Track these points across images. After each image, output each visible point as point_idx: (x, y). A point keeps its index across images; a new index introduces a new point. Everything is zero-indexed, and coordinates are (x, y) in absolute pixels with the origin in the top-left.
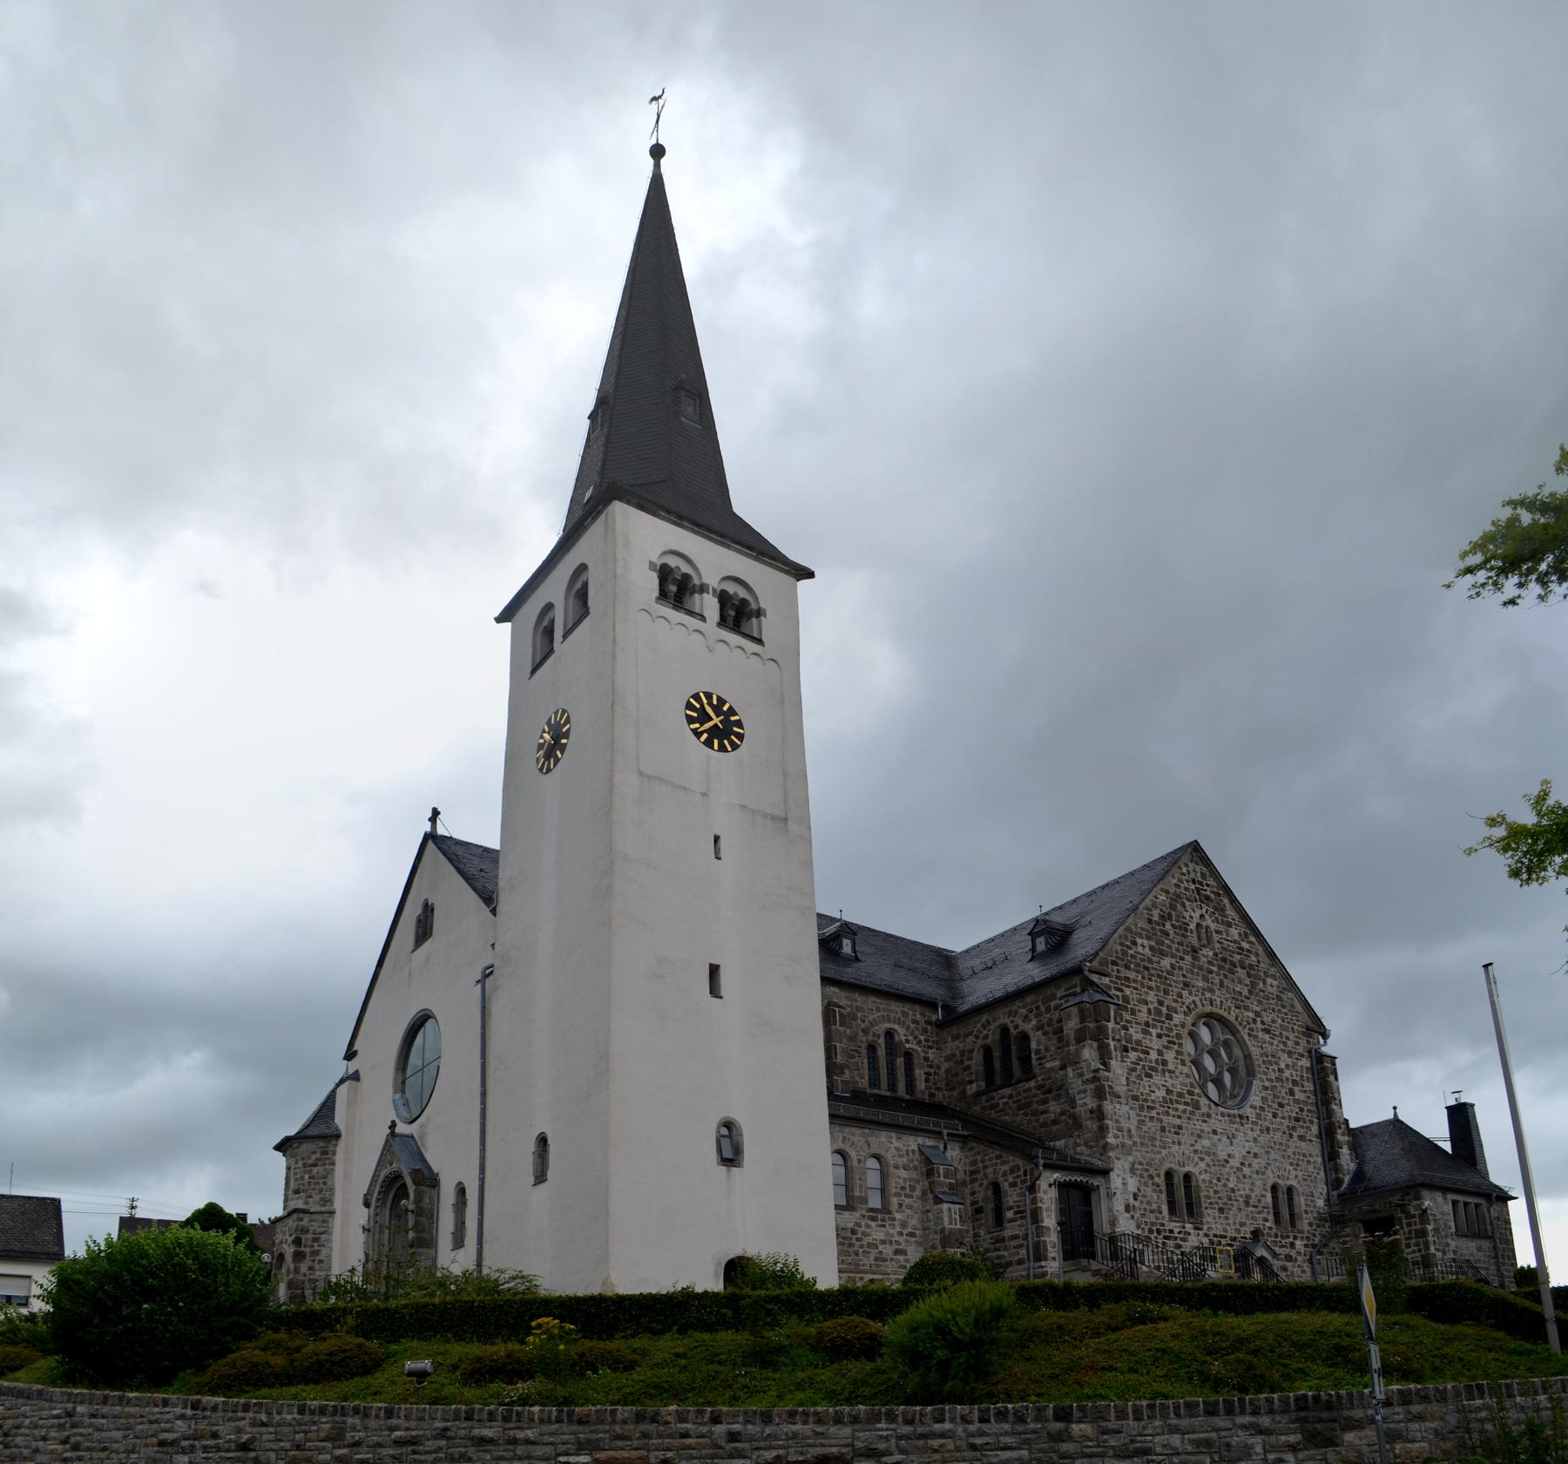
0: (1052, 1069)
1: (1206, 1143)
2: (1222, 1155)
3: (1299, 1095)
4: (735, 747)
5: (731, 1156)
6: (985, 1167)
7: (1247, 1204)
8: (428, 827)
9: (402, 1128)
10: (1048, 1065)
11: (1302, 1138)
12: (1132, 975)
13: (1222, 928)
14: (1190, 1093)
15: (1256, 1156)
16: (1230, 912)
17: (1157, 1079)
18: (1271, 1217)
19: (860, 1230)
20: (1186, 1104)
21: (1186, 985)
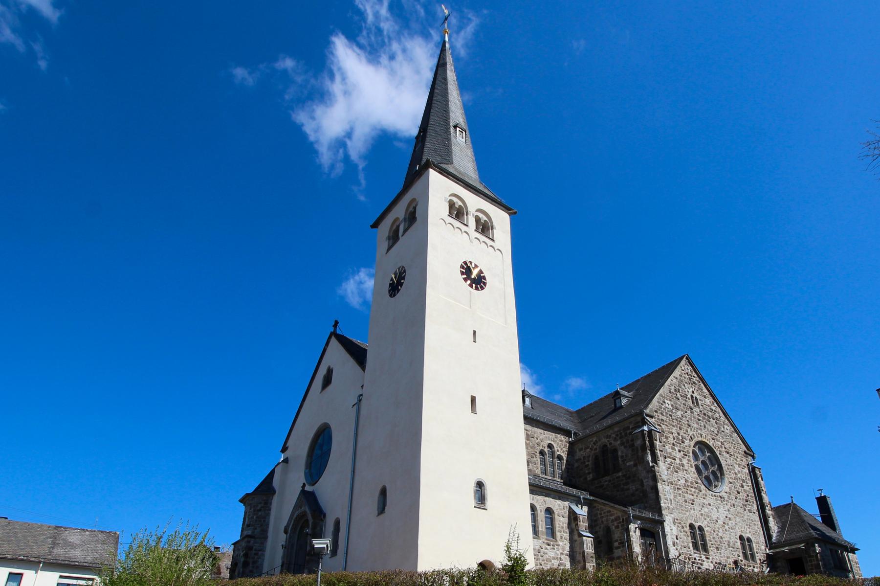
0: (629, 466)
1: (706, 510)
2: (714, 517)
3: (745, 487)
4: (482, 288)
5: (481, 498)
6: (602, 517)
7: (729, 545)
8: (332, 330)
9: (308, 488)
10: (628, 464)
11: (750, 511)
12: (664, 418)
13: (702, 398)
14: (697, 483)
15: (730, 519)
16: (705, 390)
17: (680, 474)
18: (741, 554)
19: (542, 551)
20: (695, 488)
21: (689, 425)
